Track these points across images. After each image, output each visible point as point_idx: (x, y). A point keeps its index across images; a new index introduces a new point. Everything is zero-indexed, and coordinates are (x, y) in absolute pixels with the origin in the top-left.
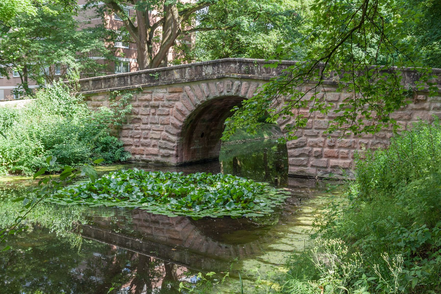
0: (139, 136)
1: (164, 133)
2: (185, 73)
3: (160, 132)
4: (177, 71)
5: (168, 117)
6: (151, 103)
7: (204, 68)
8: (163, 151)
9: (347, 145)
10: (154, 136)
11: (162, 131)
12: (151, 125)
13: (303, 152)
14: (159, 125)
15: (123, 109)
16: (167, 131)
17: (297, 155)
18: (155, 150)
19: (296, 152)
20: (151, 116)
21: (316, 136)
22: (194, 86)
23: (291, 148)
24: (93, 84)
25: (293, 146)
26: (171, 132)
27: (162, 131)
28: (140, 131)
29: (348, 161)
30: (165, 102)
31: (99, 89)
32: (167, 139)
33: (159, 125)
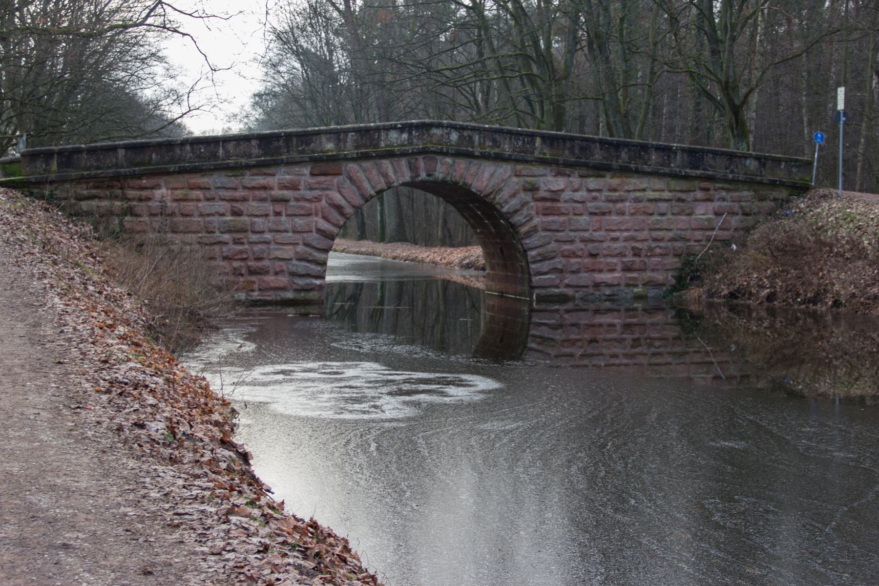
0: (245, 256)
1: (301, 248)
2: (345, 142)
3: (291, 247)
4: (328, 136)
5: (310, 219)
6: (273, 193)
7: (383, 134)
8: (301, 282)
9: (617, 251)
10: (278, 254)
11: (298, 244)
12: (272, 234)
13: (555, 266)
14: (290, 234)
15: (479, 313)
16: (306, 245)
17: (302, 273)
18: (283, 280)
19: (545, 266)
20: (272, 218)
21: (572, 242)
22: (367, 164)
23: (534, 262)
24: (125, 156)
25: (539, 258)
26: (318, 246)
27: (298, 244)
28: (246, 246)
29: (617, 275)
30: (302, 192)
31: (143, 164)
32: (310, 258)
33: (290, 234)
